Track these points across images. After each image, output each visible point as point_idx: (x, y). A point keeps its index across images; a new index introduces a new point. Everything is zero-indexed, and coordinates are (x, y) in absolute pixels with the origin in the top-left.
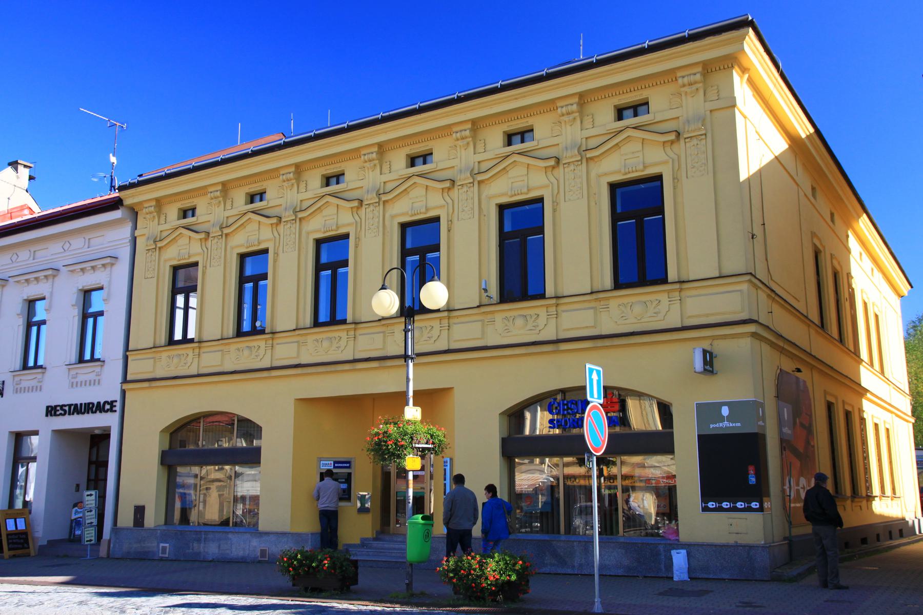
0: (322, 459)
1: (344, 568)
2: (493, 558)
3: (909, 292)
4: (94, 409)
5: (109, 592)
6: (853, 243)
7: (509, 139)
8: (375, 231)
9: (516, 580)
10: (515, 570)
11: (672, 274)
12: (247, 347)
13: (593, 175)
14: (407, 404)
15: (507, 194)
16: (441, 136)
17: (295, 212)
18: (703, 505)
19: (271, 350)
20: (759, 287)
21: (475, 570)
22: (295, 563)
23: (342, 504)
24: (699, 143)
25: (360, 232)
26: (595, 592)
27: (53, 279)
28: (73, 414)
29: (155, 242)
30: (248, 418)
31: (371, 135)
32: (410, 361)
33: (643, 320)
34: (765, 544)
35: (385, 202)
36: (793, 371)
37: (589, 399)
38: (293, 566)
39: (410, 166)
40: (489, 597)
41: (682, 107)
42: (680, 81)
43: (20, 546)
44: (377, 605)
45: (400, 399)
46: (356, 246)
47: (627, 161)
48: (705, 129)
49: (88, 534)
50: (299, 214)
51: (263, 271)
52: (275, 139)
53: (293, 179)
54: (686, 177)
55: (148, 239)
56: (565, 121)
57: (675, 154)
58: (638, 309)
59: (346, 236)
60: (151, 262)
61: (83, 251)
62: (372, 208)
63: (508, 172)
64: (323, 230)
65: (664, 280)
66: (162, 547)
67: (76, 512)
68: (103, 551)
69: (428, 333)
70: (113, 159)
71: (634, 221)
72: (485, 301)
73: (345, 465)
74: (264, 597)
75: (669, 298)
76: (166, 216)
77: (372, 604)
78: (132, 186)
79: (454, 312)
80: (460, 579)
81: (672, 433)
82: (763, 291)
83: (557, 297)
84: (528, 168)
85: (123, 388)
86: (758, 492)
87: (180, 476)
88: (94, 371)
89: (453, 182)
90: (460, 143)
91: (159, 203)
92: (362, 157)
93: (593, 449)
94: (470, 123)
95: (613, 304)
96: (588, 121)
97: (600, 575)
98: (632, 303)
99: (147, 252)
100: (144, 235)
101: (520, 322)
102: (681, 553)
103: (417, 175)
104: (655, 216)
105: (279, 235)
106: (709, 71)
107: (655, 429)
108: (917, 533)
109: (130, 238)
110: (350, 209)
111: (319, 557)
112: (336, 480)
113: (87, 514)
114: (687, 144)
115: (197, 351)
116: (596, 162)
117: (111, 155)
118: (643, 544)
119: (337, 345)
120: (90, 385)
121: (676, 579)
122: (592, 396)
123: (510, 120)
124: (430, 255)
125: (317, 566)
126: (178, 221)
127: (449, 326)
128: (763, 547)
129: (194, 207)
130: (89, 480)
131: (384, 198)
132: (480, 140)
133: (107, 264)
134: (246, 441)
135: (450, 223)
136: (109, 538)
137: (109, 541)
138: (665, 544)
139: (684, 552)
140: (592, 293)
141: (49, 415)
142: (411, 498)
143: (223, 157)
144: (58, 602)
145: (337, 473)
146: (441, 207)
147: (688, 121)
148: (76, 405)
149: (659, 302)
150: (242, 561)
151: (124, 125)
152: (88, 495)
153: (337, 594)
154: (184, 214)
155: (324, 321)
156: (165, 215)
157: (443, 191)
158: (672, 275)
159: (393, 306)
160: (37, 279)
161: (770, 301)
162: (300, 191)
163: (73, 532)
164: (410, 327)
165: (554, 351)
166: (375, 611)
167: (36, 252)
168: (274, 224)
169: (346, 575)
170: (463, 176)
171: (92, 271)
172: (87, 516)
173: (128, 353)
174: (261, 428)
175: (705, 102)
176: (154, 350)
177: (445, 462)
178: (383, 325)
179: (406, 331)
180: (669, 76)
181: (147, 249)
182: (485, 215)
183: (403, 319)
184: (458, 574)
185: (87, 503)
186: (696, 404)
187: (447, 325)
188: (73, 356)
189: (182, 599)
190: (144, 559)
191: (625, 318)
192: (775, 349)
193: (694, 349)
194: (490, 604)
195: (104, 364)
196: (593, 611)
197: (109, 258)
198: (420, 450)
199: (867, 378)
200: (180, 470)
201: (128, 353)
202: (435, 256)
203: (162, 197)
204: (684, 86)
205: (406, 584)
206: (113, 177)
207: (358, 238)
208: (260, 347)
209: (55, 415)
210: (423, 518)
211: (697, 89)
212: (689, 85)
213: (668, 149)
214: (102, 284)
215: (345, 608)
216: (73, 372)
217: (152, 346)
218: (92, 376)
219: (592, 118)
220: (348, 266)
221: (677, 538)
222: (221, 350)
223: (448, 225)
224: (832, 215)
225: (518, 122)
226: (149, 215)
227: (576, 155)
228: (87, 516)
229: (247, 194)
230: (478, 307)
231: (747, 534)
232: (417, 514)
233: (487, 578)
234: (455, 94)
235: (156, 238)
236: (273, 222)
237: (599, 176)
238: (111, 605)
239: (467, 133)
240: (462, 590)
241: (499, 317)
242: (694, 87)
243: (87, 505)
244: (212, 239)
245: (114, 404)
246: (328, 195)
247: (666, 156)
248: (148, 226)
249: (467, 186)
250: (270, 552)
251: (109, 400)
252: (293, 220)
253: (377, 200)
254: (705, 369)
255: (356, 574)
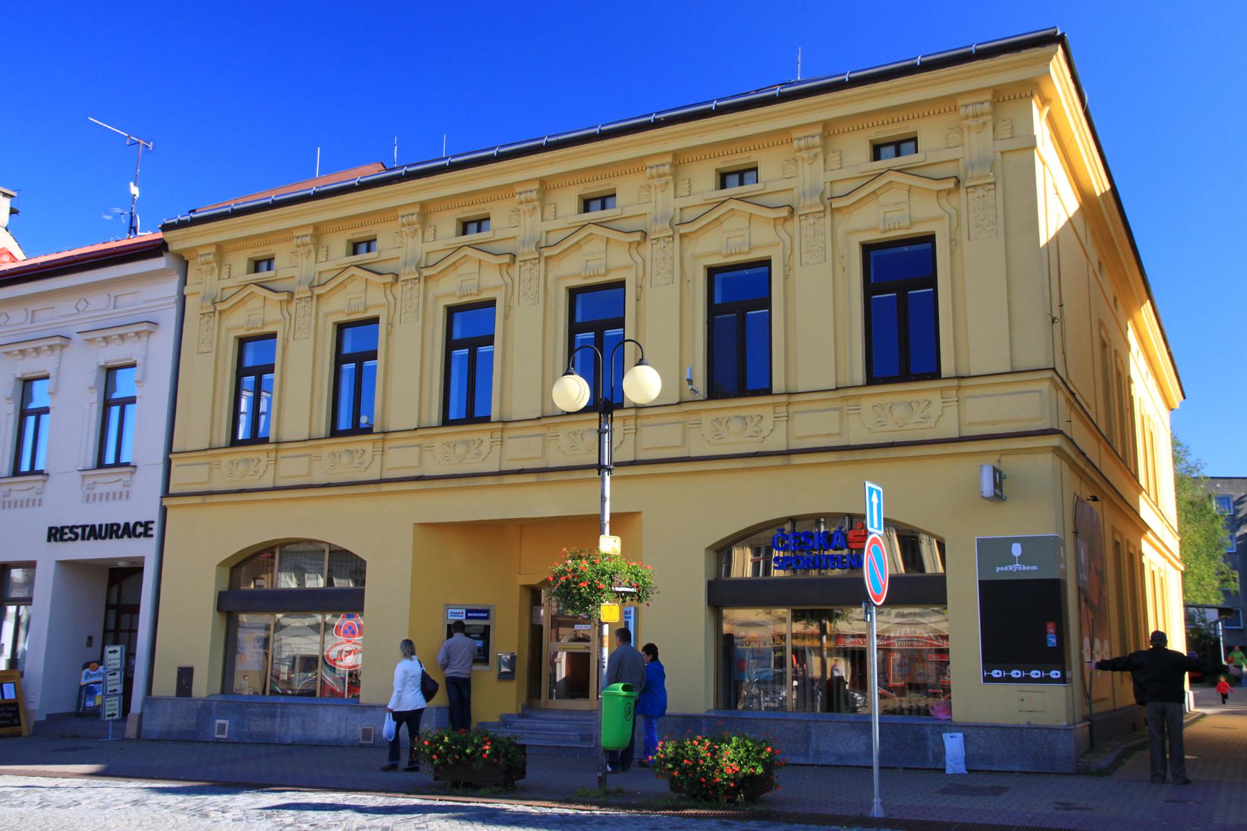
0: (450, 607)
1: (510, 756)
2: (729, 742)
3: (1181, 404)
4: (120, 533)
5: (169, 788)
6: (1131, 336)
7: (723, 179)
8: (208, 345)
9: (762, 774)
10: (760, 759)
11: (947, 366)
12: (347, 450)
13: (840, 230)
14: (602, 532)
15: (878, 229)
16: (628, 172)
17: (419, 268)
18: (985, 674)
19: (499, 446)
20: (1061, 388)
21: (704, 759)
22: (441, 748)
23: (476, 667)
24: (985, 194)
25: (511, 297)
26: (873, 790)
27: (148, 337)
28: (88, 539)
29: (214, 303)
30: (346, 548)
31: (531, 167)
32: (607, 473)
33: (907, 427)
34: (1068, 725)
35: (547, 258)
36: (1088, 500)
37: (870, 529)
38: (438, 752)
39: (253, 271)
40: (725, 797)
41: (963, 145)
42: (962, 111)
43: (8, 722)
44: (566, 806)
45: (592, 525)
46: (506, 317)
47: (887, 215)
48: (995, 176)
49: (110, 705)
50: (424, 271)
51: (371, 348)
52: (372, 171)
53: (417, 224)
54: (967, 240)
55: (204, 298)
56: (656, 186)
57: (953, 207)
58: (899, 412)
59: (491, 303)
60: (207, 330)
61: (24, 326)
62: (529, 265)
63: (722, 223)
64: (458, 294)
65: (935, 374)
66: (219, 724)
67: (88, 675)
68: (131, 729)
69: (477, 448)
70: (135, 190)
71: (895, 294)
72: (688, 395)
73: (482, 615)
74: (397, 795)
75: (942, 398)
76: (230, 269)
77: (557, 805)
78: (182, 225)
79: (509, 423)
80: (684, 771)
81: (364, 590)
82: (1063, 393)
83: (789, 394)
84: (750, 219)
85: (164, 504)
86: (1056, 658)
87: (243, 627)
88: (33, 487)
89: (645, 234)
90: (656, 182)
91: (221, 250)
92: (517, 196)
93: (873, 597)
94: (418, 206)
95: (866, 404)
96: (833, 160)
97: (881, 768)
98: (729, 418)
99: (202, 316)
100: (198, 293)
101: (736, 425)
102: (956, 737)
103: (737, 199)
104: (925, 288)
105: (395, 299)
106: (1001, 99)
107: (896, 573)
108: (1187, 711)
109: (177, 297)
110: (498, 267)
111: (476, 741)
112: (468, 635)
113: (109, 678)
114: (969, 194)
115: (273, 455)
116: (845, 214)
117: (132, 184)
118: (903, 725)
119: (477, 451)
120: (21, 506)
121: (949, 771)
122: (872, 526)
123: (725, 153)
124: (482, 349)
125: (473, 753)
126: (249, 276)
127: (636, 429)
128: (1067, 730)
129: (272, 257)
130: (106, 631)
131: (547, 253)
132: (683, 180)
133: (143, 331)
134: (353, 582)
135: (639, 289)
136: (139, 712)
137: (141, 716)
138: (934, 725)
139: (960, 735)
140: (837, 389)
141: (52, 539)
142: (606, 660)
143: (317, 190)
144: (100, 801)
145: (469, 626)
146: (628, 267)
147: (972, 165)
148: (93, 527)
149: (929, 403)
150: (335, 745)
151: (150, 144)
152: (110, 652)
153: (501, 792)
154: (256, 265)
155: (456, 418)
156: (228, 266)
157: (630, 247)
158: (947, 367)
159: (583, 398)
160: (37, 350)
161: (1068, 409)
162: (319, 260)
163: (82, 704)
164: (607, 427)
165: (784, 465)
166: (567, 815)
167: (36, 313)
168: (388, 283)
169: (513, 765)
170: (526, 250)
171: (120, 342)
172: (109, 681)
173: (171, 456)
174: (365, 562)
175: (994, 140)
176: (210, 452)
177: (626, 613)
178: (544, 425)
179: (601, 433)
180: (947, 103)
181: (202, 312)
182: (689, 281)
183: (596, 416)
184: (679, 765)
185: (109, 663)
186: (978, 540)
187: (634, 427)
188: (90, 459)
189: (281, 798)
190: (192, 741)
191: (882, 423)
192: (1074, 471)
193: (982, 466)
194: (726, 807)
195: (136, 470)
196: (870, 815)
197: (146, 324)
198: (622, 596)
199: (1146, 512)
200: (244, 618)
201: (171, 456)
202: (617, 333)
203: (683, 149)
204: (967, 117)
205: (599, 777)
206: (133, 215)
207: (508, 307)
208: (364, 451)
209: (62, 540)
210: (624, 688)
211: (985, 123)
212: (974, 117)
213: (943, 201)
214: (134, 359)
215: (521, 810)
216: (89, 481)
217: (207, 447)
218: (117, 487)
219: (840, 155)
220: (273, 373)
221: (949, 717)
222: (309, 455)
223: (637, 292)
224: (1115, 299)
225: (741, 157)
226: (301, 248)
227: (817, 205)
228: (109, 681)
229: (250, 259)
230: (678, 403)
231: (1043, 712)
232: (616, 682)
233: (722, 771)
234: (597, 127)
235: (216, 297)
236: (387, 281)
237: (848, 234)
238: (183, 806)
239: (667, 169)
240: (685, 787)
241: (706, 419)
242: (981, 120)
243: (110, 665)
244: (297, 301)
245: (150, 526)
246: (468, 246)
247: (777, 236)
248: (202, 282)
249: (664, 240)
250: (376, 732)
251: (143, 520)
252: (415, 279)
253: (537, 256)
254: (995, 494)
255: (525, 764)
